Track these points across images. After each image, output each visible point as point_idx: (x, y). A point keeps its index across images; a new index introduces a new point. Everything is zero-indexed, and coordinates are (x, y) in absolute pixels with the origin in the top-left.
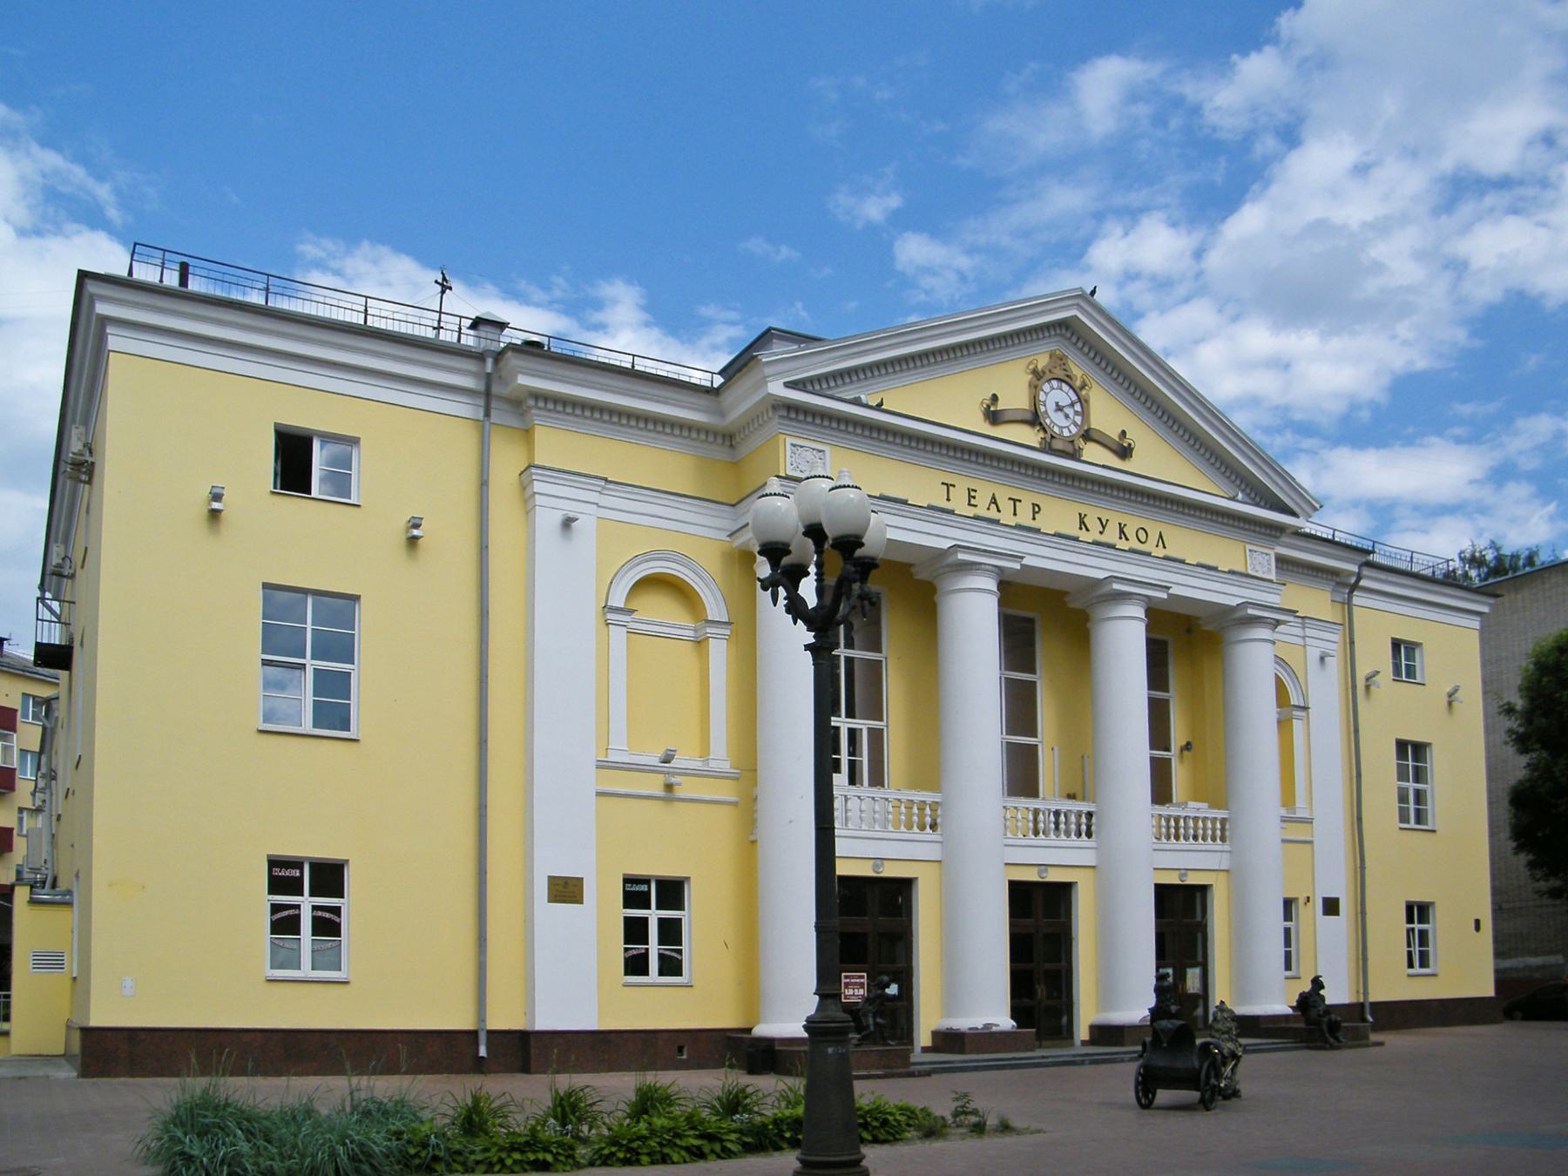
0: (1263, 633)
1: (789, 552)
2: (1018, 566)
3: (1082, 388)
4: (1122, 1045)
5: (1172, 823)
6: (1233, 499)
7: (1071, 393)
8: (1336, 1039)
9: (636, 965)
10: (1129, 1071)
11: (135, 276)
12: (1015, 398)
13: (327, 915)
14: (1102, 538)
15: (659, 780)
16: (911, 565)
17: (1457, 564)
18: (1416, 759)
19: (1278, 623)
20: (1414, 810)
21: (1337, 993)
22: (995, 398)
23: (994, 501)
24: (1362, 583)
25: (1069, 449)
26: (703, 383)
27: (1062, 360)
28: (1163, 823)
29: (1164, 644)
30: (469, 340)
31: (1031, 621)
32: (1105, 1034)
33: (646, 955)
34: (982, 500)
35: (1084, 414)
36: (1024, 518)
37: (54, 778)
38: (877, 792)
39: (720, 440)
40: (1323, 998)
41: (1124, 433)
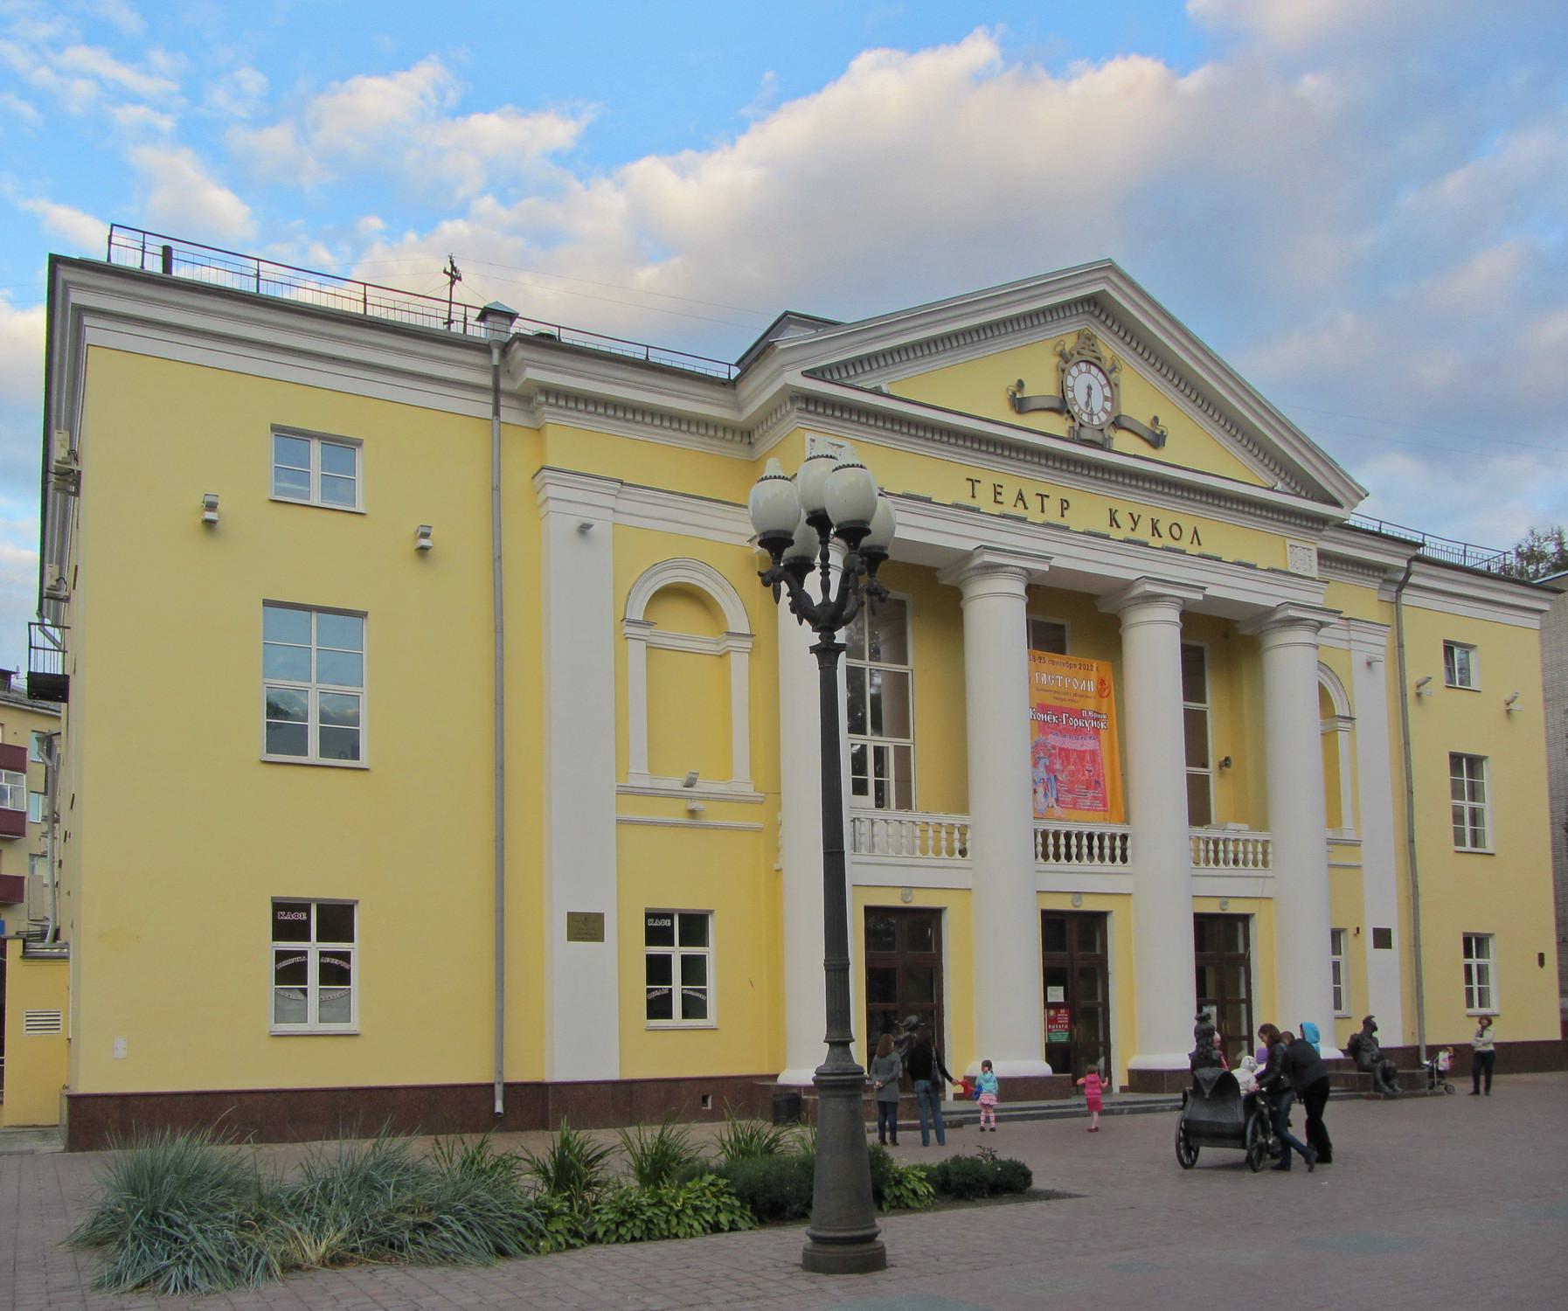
0: (1302, 635)
1: (791, 543)
2: (1047, 568)
3: (1113, 370)
4: (1163, 1092)
5: (1211, 846)
6: (1272, 489)
7: (1100, 376)
8: (1391, 1087)
9: (658, 1008)
10: (1168, 1124)
11: (114, 261)
12: (1041, 385)
13: (336, 961)
14: (1133, 536)
15: (683, 805)
16: (936, 569)
17: (1512, 560)
18: (1471, 774)
19: (1322, 624)
20: (1468, 829)
21: (1390, 1036)
22: (1020, 384)
23: (1021, 497)
24: (1412, 580)
25: (1099, 438)
26: (721, 375)
27: (1087, 339)
28: (1202, 846)
29: (1200, 650)
30: (478, 331)
31: (1061, 628)
32: (1144, 1080)
33: (669, 996)
34: (1009, 496)
35: (1113, 399)
36: (1053, 515)
37: (57, 821)
38: (904, 815)
39: (738, 438)
40: (1376, 1041)
41: (1156, 419)
